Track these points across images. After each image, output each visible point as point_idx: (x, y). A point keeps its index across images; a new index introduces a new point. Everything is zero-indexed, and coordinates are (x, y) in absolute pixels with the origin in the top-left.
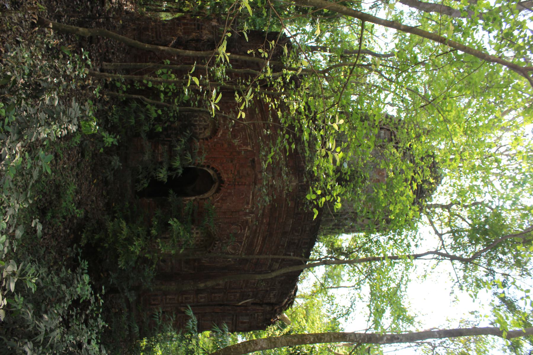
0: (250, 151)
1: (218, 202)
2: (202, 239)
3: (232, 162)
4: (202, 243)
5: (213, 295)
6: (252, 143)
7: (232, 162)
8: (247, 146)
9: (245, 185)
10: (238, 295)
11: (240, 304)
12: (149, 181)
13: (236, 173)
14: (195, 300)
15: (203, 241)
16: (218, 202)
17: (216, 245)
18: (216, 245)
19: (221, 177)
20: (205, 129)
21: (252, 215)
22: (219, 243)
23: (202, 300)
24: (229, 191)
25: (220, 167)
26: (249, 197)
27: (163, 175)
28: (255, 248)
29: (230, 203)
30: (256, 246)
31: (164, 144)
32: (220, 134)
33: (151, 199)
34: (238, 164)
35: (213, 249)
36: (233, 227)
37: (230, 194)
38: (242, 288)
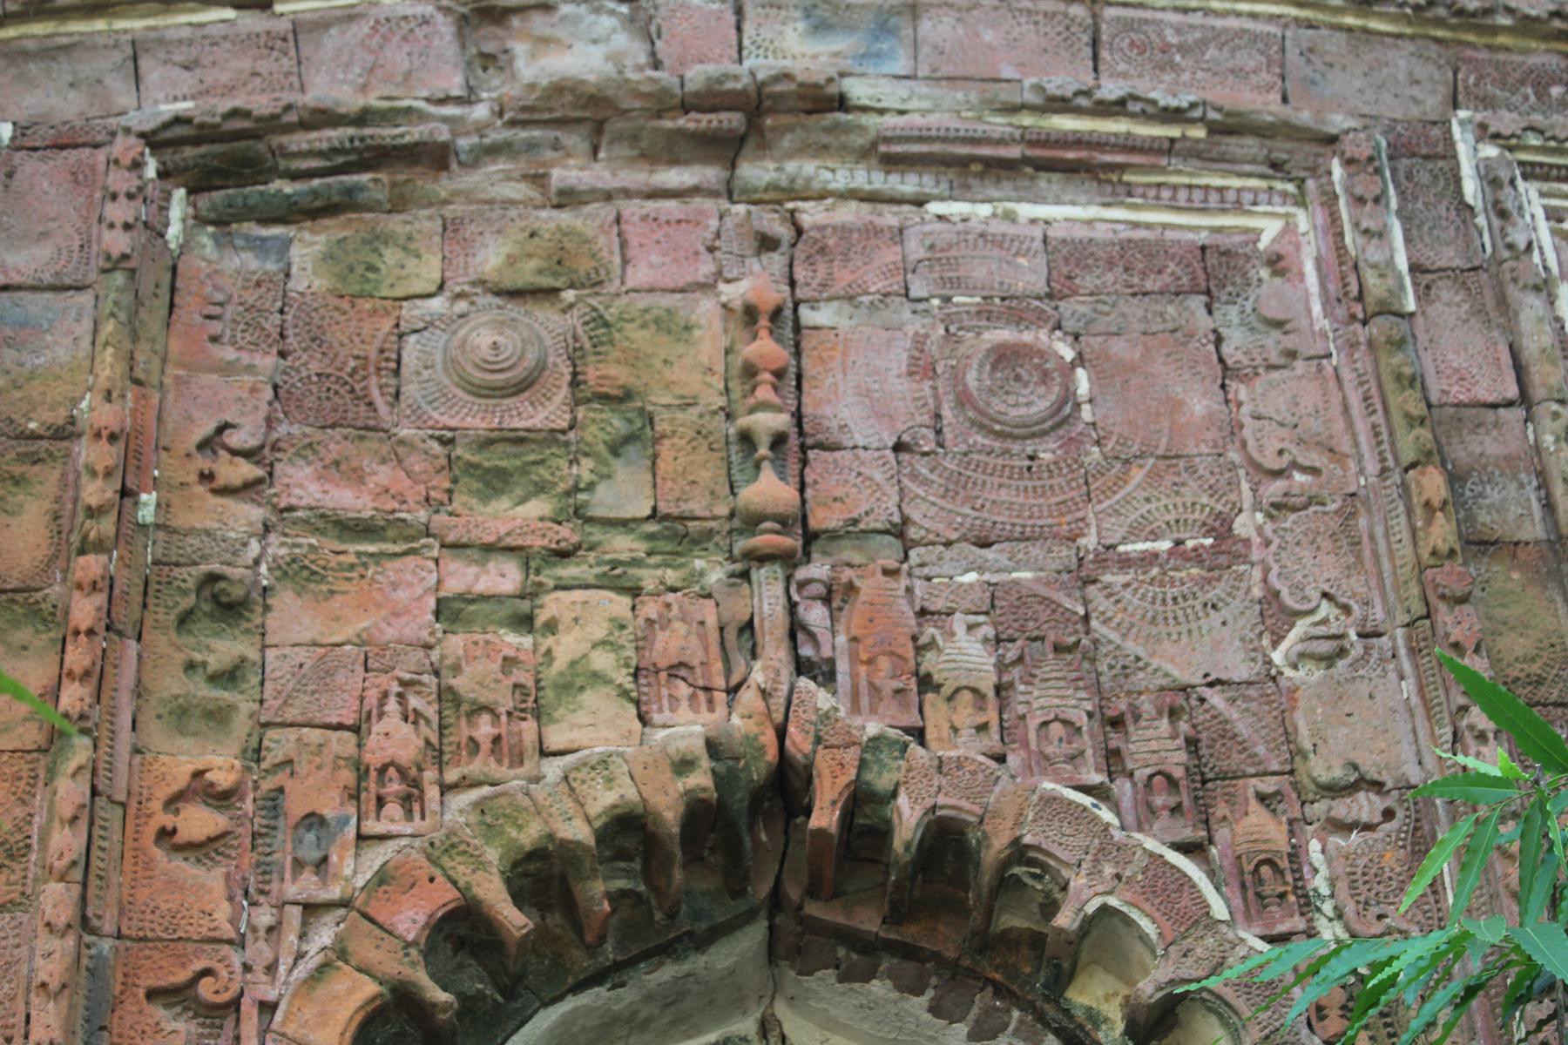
3: (227, 605)
7: (227, 605)
13: (523, 515)
24: (966, 653)
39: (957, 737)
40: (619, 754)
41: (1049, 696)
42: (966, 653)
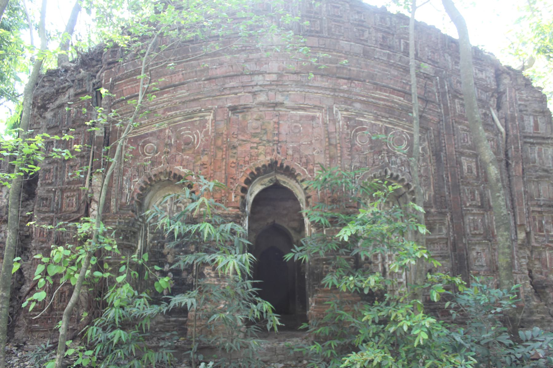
0: (215, 116)
1: (311, 171)
3: (235, 147)
7: (235, 147)
8: (206, 121)
13: (257, 140)
24: (290, 152)
26: (301, 117)
36: (358, 142)
39: (289, 159)
40: (264, 160)
42: (290, 152)
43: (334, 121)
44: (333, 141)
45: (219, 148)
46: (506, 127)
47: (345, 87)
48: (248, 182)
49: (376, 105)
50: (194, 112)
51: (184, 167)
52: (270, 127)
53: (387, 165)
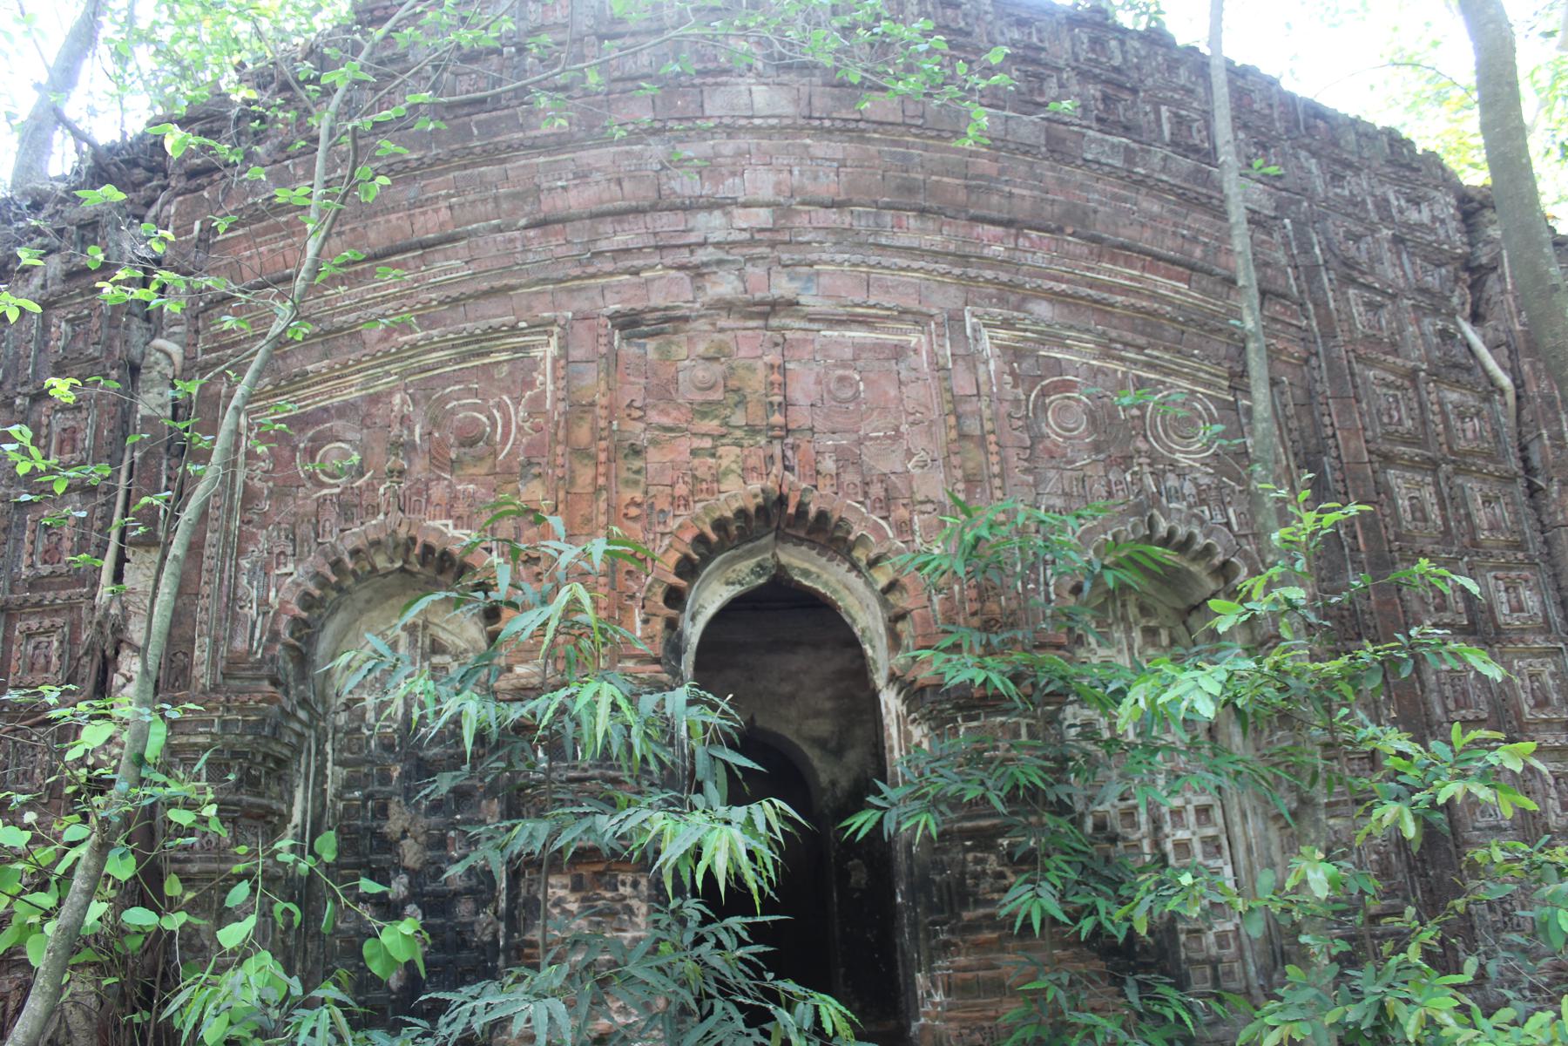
0: (564, 347)
1: (904, 528)
2: (1137, 635)
3: (636, 452)
4: (1164, 639)
5: (1482, 536)
6: (513, 329)
7: (636, 452)
8: (535, 364)
9: (783, 370)
10: (1453, 396)
11: (1505, 381)
12: (790, 986)
13: (712, 425)
14: (1539, 642)
15: (1151, 633)
16: (904, 528)
17: (1182, 531)
18: (1182, 531)
19: (741, 513)
20: (437, 648)
21: (969, 321)
22: (1167, 514)
23: (1530, 599)
24: (828, 465)
25: (673, 524)
26: (859, 348)
27: (730, 838)
28: (1163, 299)
29: (909, 454)
30: (1154, 296)
31: (534, 907)
32: (452, 532)
33: (920, 978)
34: (654, 417)
35: (1208, 551)
36: (1051, 426)
37: (846, 458)
38: (1412, 375)
39: (826, 488)
41: (850, 477)
42: (828, 465)
43: (972, 360)
44: (972, 426)
45: (582, 453)
46: (1519, 385)
47: (998, 250)
48: (688, 569)
49: (1101, 308)
50: (493, 333)
51: (459, 521)
52: (756, 383)
53: (1155, 500)
